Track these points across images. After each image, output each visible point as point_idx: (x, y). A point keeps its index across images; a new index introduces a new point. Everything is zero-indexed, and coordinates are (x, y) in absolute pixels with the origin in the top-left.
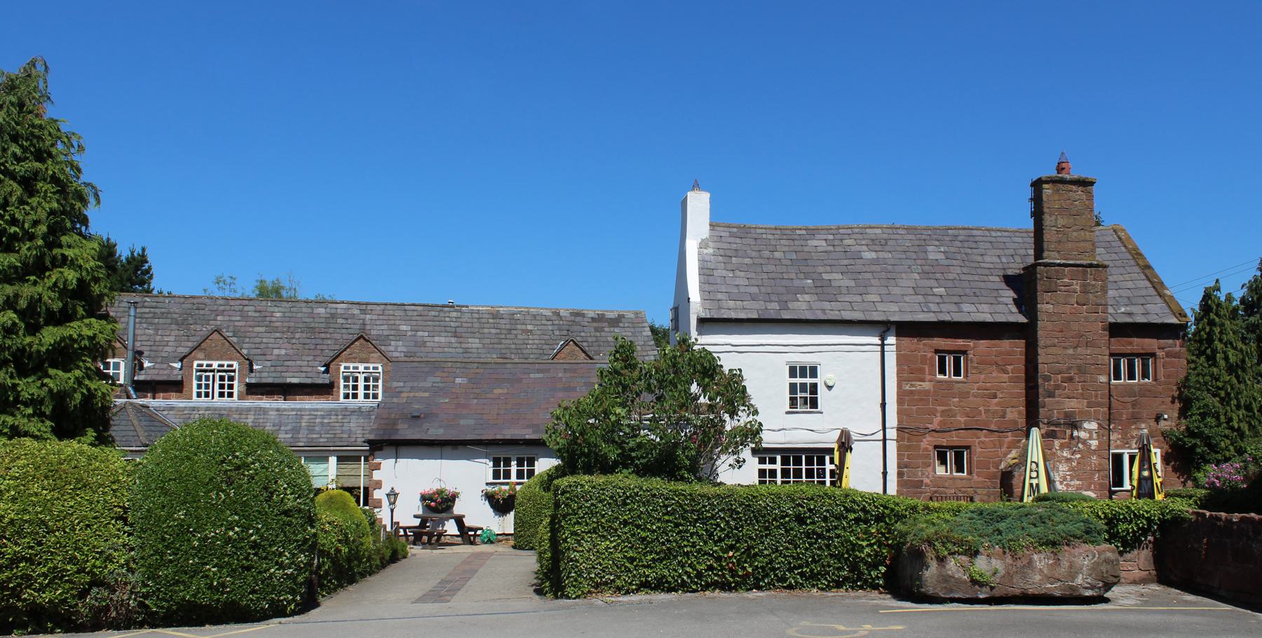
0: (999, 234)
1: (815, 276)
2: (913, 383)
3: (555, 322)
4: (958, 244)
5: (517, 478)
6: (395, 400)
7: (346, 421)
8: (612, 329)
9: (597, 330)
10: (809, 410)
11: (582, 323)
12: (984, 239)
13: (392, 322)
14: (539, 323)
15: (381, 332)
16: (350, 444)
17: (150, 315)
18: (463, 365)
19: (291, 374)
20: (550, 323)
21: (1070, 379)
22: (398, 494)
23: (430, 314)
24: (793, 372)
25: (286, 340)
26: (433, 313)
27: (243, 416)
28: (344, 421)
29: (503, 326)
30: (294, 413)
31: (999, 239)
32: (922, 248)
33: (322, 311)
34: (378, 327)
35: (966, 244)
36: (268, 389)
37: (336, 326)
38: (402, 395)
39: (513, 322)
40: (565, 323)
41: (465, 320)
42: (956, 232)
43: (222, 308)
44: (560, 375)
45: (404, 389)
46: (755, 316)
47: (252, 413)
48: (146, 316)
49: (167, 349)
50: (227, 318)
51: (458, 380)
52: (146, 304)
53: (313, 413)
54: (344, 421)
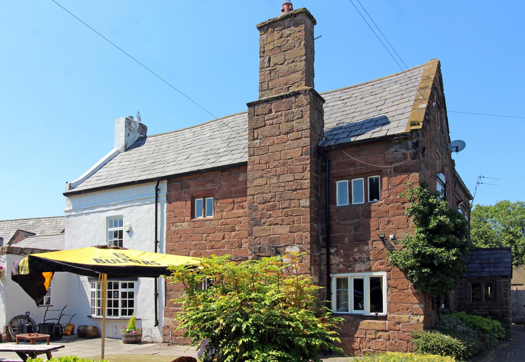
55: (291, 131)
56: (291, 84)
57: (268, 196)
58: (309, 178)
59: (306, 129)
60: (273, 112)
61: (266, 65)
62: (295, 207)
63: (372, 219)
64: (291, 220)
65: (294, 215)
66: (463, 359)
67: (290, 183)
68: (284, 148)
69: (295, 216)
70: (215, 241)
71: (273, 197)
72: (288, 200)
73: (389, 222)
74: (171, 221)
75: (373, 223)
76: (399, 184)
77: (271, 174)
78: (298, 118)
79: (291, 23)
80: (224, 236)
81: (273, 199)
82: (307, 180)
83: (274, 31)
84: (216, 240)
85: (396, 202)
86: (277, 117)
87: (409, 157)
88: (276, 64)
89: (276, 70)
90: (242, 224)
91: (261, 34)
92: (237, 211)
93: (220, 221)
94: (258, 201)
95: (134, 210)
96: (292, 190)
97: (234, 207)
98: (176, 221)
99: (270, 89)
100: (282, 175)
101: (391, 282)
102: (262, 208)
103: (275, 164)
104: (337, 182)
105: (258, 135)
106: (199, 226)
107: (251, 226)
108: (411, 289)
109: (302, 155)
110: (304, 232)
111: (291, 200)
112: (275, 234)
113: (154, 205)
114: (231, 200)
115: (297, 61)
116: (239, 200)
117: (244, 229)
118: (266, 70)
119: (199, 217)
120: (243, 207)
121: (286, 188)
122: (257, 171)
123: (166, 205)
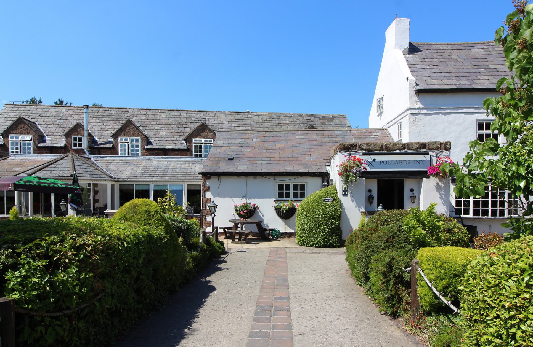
1: (484, 67)
3: (300, 120)
5: (294, 198)
6: (218, 150)
7: (193, 166)
8: (330, 123)
9: (322, 123)
11: (314, 121)
13: (219, 120)
14: (292, 120)
15: (213, 124)
16: (194, 178)
17: (101, 116)
18: (257, 132)
19: (168, 144)
20: (298, 120)
22: (217, 206)
23: (238, 116)
24: (480, 127)
25: (166, 128)
26: (239, 116)
27: (139, 164)
28: (192, 166)
29: (274, 122)
30: (167, 162)
33: (185, 114)
34: (212, 122)
36: (156, 151)
37: (191, 122)
38: (223, 148)
40: (305, 120)
41: (255, 119)
43: (136, 113)
44: (314, 137)
45: (224, 145)
46: (455, 87)
47: (144, 162)
48: (99, 117)
49: (107, 132)
50: (138, 118)
51: (255, 140)
52: (99, 111)
53: (176, 162)
54: (192, 166)
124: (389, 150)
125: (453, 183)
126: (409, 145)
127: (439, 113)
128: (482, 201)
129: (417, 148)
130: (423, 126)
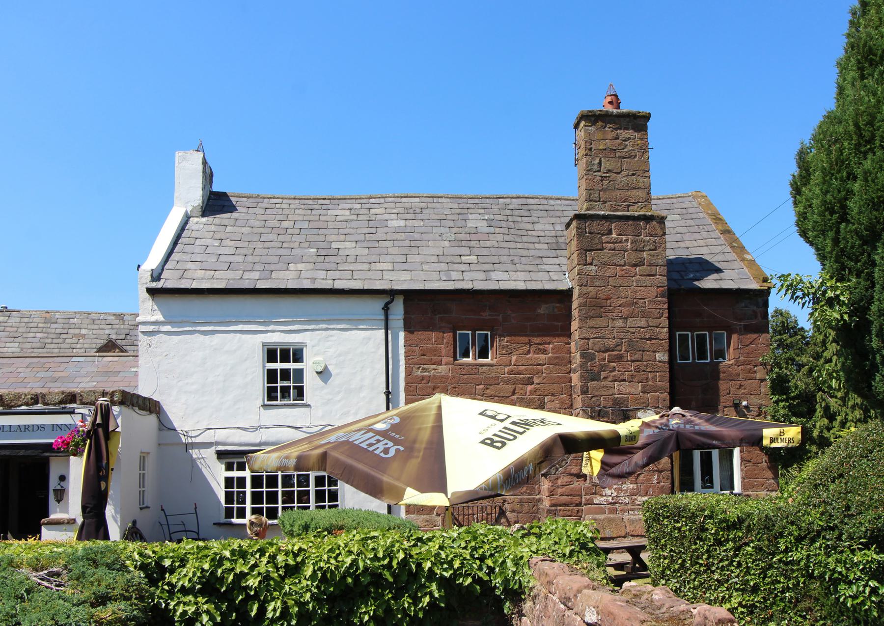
0: (559, 202)
2: (426, 366)
4: (508, 212)
10: (292, 402)
12: (541, 207)
21: (619, 359)
24: (271, 355)
31: (556, 208)
32: (463, 215)
35: (516, 213)
39: (66, 326)
42: (508, 201)
55: (641, 264)
56: (633, 203)
57: (611, 343)
58: (668, 326)
59: (662, 266)
60: (614, 233)
61: (595, 167)
62: (650, 361)
63: (721, 382)
64: (644, 376)
65: (648, 370)
66: (347, 585)
67: (642, 330)
68: (631, 284)
69: (649, 372)
70: (499, 397)
71: (619, 345)
72: (639, 351)
73: (741, 386)
74: (417, 359)
75: (723, 385)
76: (749, 345)
77: (614, 314)
78: (650, 250)
79: (630, 124)
80: (515, 390)
81: (619, 348)
82: (665, 329)
83: (605, 127)
84: (502, 395)
85: (747, 365)
86: (620, 242)
87: (759, 315)
88: (609, 171)
89: (610, 179)
90: (544, 375)
91: (587, 124)
92: (536, 356)
93: (508, 368)
94: (596, 348)
95: (331, 336)
96: (645, 339)
97: (529, 350)
98: (425, 363)
99: (603, 201)
100: (630, 317)
101: (745, 455)
102: (601, 357)
103: (620, 303)
104: (678, 333)
105: (593, 260)
106: (469, 373)
107: (585, 380)
108: (766, 462)
109: (657, 297)
110: (661, 393)
111: (644, 351)
112: (622, 394)
113: (383, 331)
114: (525, 339)
115: (639, 176)
116: (538, 340)
117: (547, 382)
118: (595, 174)
119: (464, 359)
120: (545, 351)
121: (637, 336)
122: (593, 308)
123: (402, 335)
124: (8, 405)
125: (221, 460)
126: (45, 396)
127: (195, 330)
128: (298, 491)
129: (61, 403)
130: (165, 354)
